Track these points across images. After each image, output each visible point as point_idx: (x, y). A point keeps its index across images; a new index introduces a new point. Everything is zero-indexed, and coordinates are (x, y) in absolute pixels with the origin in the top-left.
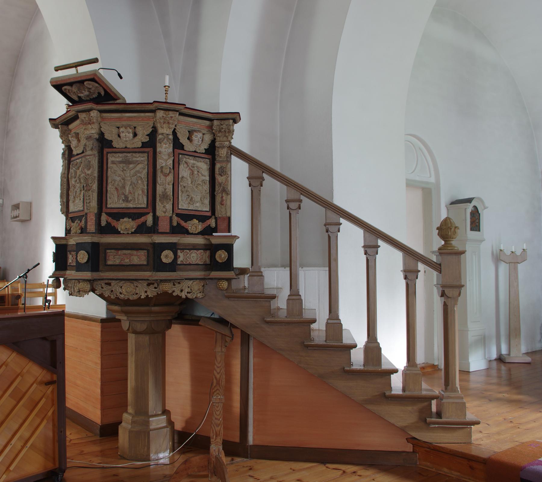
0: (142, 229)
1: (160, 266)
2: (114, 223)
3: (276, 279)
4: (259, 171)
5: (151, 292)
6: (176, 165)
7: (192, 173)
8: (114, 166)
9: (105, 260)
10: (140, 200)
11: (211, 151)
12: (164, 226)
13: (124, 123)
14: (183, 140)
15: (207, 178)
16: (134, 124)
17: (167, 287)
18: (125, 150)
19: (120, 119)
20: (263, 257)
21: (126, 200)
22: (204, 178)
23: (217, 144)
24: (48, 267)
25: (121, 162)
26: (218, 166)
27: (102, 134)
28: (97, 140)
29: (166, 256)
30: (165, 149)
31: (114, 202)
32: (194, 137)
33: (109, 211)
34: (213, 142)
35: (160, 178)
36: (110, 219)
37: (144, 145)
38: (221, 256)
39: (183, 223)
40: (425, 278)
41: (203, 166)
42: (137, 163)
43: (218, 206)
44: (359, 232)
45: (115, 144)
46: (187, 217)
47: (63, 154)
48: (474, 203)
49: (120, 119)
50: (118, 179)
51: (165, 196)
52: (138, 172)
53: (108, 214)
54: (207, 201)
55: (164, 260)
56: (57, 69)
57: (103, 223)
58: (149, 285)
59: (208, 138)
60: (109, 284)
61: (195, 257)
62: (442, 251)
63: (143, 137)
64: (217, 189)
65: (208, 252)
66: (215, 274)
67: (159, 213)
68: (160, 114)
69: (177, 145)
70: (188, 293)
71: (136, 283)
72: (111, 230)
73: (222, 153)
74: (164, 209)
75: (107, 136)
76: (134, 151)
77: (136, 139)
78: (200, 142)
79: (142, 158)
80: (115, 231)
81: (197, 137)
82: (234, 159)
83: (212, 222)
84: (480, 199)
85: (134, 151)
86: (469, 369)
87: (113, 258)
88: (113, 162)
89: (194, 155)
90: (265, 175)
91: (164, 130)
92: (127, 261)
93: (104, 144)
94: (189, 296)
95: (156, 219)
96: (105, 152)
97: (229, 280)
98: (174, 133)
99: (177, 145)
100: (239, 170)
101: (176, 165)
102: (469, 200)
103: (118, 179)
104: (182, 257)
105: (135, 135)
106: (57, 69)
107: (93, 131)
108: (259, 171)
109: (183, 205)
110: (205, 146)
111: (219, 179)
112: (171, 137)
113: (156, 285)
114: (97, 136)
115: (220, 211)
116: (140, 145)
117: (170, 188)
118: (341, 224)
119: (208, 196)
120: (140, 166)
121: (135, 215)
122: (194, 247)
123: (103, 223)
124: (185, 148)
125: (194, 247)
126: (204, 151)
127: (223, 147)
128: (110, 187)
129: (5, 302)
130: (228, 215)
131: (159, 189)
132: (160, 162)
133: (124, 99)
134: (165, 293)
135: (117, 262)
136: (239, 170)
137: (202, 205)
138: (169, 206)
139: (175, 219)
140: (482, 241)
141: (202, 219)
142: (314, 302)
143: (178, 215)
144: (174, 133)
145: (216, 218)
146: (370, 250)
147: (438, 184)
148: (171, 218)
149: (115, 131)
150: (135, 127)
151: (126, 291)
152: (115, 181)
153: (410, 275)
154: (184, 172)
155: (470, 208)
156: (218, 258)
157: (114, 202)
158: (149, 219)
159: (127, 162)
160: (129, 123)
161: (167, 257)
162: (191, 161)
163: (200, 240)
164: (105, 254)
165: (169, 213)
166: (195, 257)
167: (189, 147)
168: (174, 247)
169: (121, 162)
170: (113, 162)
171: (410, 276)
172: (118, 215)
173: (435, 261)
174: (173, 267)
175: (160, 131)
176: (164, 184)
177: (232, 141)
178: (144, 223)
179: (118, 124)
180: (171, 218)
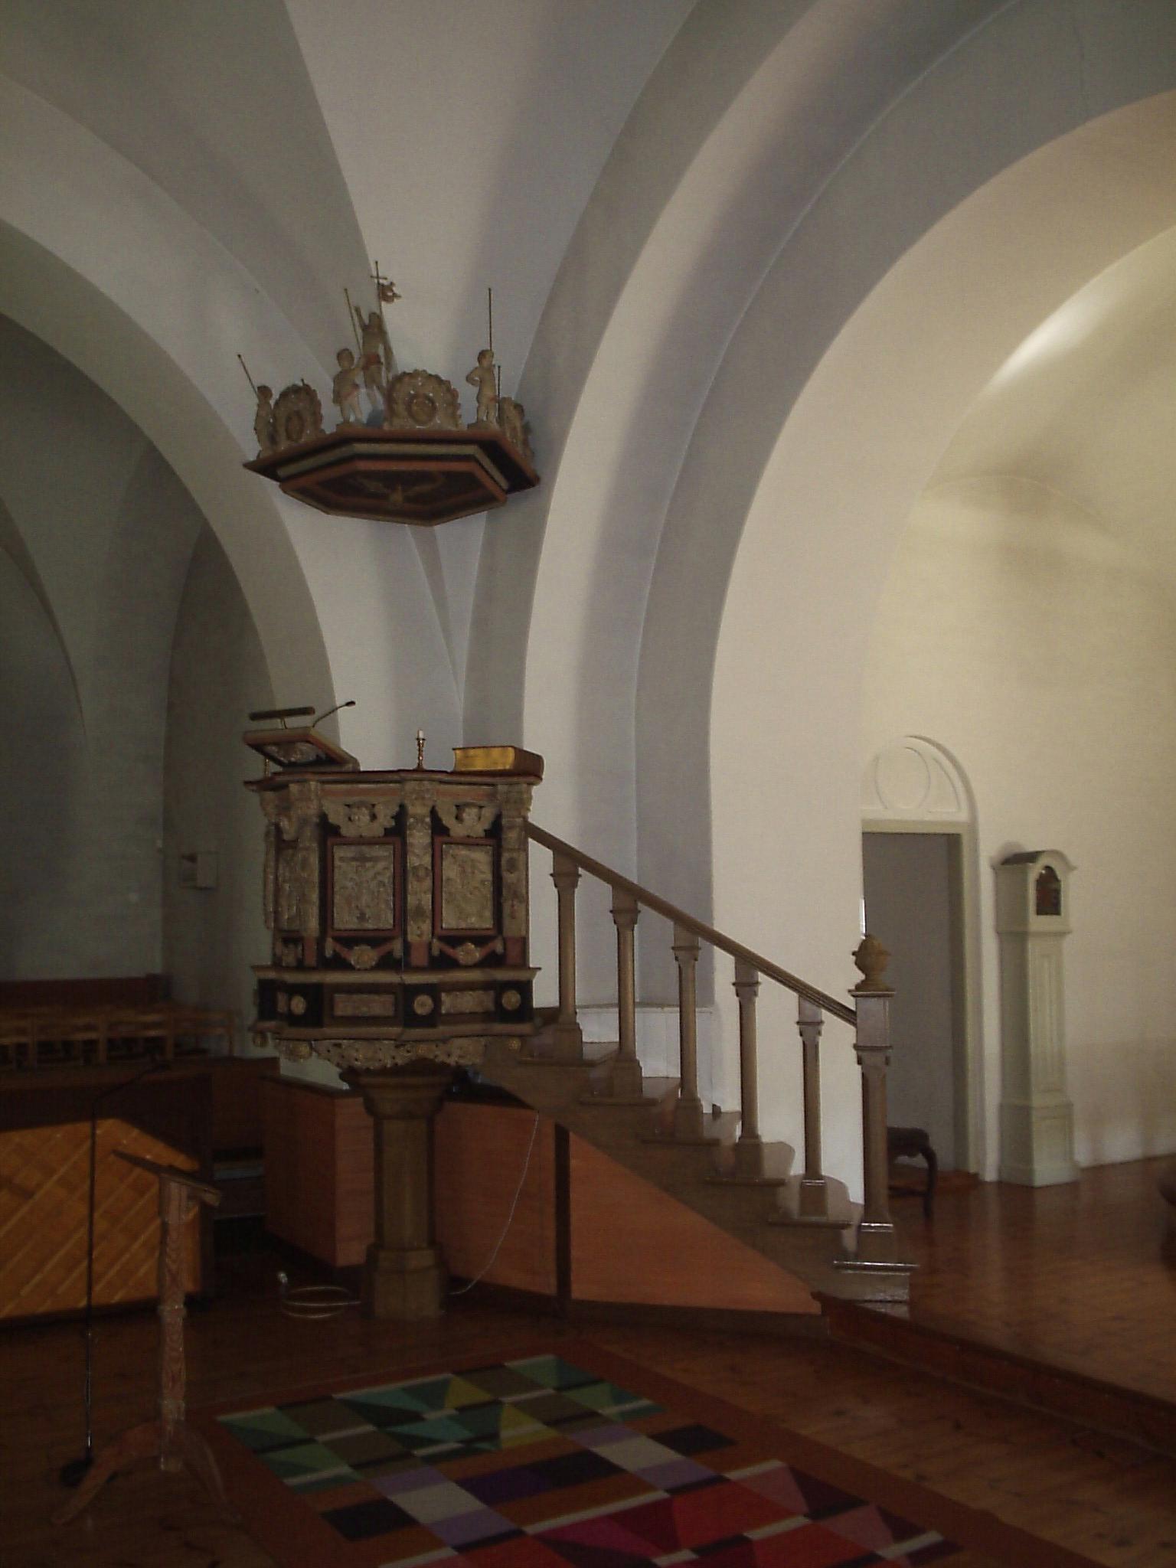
0: (387, 963)
1: (411, 1020)
2: (344, 952)
4: (570, 864)
5: (402, 1057)
6: (436, 858)
7: (464, 871)
8: (344, 865)
9: (332, 1008)
11: (495, 833)
12: (419, 958)
13: (356, 799)
14: (448, 820)
15: (489, 876)
16: (372, 800)
17: (422, 1050)
18: (361, 841)
19: (349, 793)
20: (580, 996)
21: (362, 917)
22: (483, 876)
23: (504, 821)
24: (251, 1013)
25: (354, 859)
26: (506, 856)
27: (323, 817)
28: (318, 825)
29: (423, 1005)
30: (419, 838)
31: (345, 919)
32: (465, 816)
33: (337, 934)
34: (498, 818)
35: (413, 885)
36: (338, 948)
37: (388, 832)
38: (511, 999)
39: (449, 951)
41: (481, 858)
42: (375, 860)
43: (507, 921)
45: (344, 831)
46: (455, 939)
47: (267, 834)
48: (1043, 861)
49: (349, 793)
50: (350, 884)
51: (419, 911)
52: (379, 873)
53: (337, 939)
54: (488, 914)
55: (419, 1011)
56: (255, 717)
57: (329, 953)
58: (397, 1047)
59: (488, 813)
60: (339, 1046)
61: (468, 1002)
62: (859, 991)
63: (385, 820)
64: (505, 892)
65: (492, 993)
66: (498, 1028)
68: (410, 786)
69: (438, 829)
70: (460, 1057)
71: (377, 1044)
73: (511, 836)
74: (419, 931)
75: (333, 819)
76: (371, 842)
77: (376, 824)
78: (474, 823)
79: (384, 852)
80: (454, 964)
81: (470, 814)
82: (532, 842)
83: (498, 947)
84: (1057, 854)
85: (371, 842)
86: (1030, 1173)
87: (344, 1006)
88: (341, 859)
89: (469, 842)
90: (581, 871)
91: (418, 810)
92: (364, 1010)
93: (328, 831)
94: (462, 1062)
95: (407, 947)
96: (329, 843)
97: (521, 1037)
98: (433, 813)
99: (438, 829)
100: (540, 860)
101: (436, 858)
102: (1033, 857)
103: (350, 884)
104: (448, 1002)
105: (374, 817)
106: (255, 717)
107: (312, 810)
108: (570, 864)
109: (450, 921)
111: (509, 877)
112: (428, 820)
113: (408, 1047)
114: (315, 820)
115: (510, 928)
116: (381, 832)
117: (427, 898)
118: (699, 949)
119: (490, 904)
120: (380, 866)
121: (374, 939)
122: (470, 986)
123: (329, 953)
124: (452, 833)
125: (470, 986)
126: (482, 834)
127: (511, 827)
128: (337, 899)
130: (523, 933)
131: (411, 900)
132: (413, 861)
133: (355, 762)
134: (423, 1060)
135: (349, 1012)
136: (540, 860)
137: (480, 919)
138: (426, 926)
139: (437, 945)
140: (1061, 934)
141: (480, 940)
143: (441, 938)
144: (433, 813)
145: (505, 941)
146: (745, 989)
147: (973, 825)
148: (430, 945)
149: (343, 811)
150: (374, 805)
151: (361, 1055)
152: (344, 888)
154: (450, 870)
155: (1035, 871)
156: (509, 1002)
157: (345, 919)
158: (397, 947)
159: (362, 859)
160: (363, 798)
161: (423, 1005)
162: (463, 852)
164: (332, 1000)
165: (427, 936)
166: (468, 1002)
167: (457, 830)
168: (433, 991)
169: (354, 859)
170: (341, 859)
171: (809, 1030)
172: (350, 940)
173: (824, 1011)
174: (431, 1019)
175: (411, 810)
176: (419, 894)
177: (529, 814)
178: (390, 953)
179: (350, 800)
180: (430, 945)
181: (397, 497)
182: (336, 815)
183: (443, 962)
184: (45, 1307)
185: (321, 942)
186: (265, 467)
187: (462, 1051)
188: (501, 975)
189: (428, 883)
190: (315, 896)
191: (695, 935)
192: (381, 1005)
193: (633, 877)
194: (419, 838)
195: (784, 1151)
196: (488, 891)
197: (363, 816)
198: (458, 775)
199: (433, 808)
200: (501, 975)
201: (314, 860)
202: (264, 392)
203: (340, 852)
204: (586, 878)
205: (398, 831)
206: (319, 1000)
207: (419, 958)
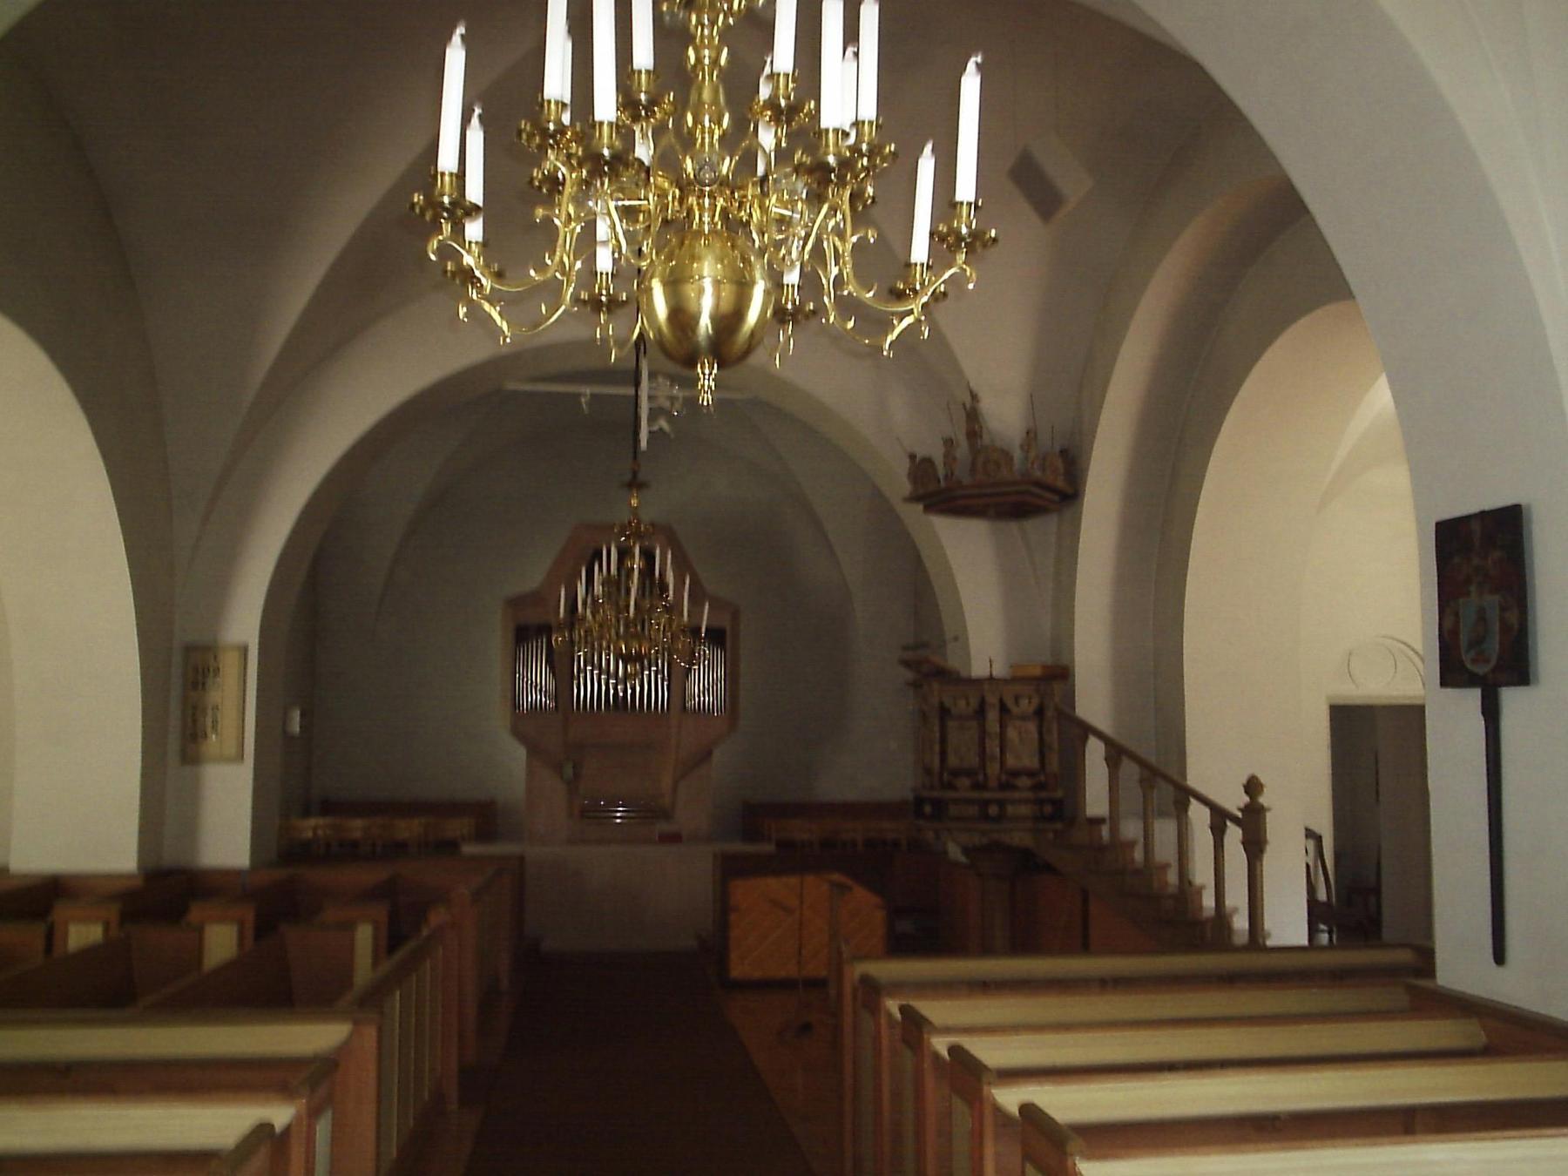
0: (977, 786)
1: (986, 817)
3: (1131, 829)
4: (1116, 754)
5: (985, 841)
6: (1002, 726)
10: (973, 760)
11: (1040, 712)
12: (993, 783)
14: (1010, 703)
30: (992, 716)
31: (953, 761)
40: (1234, 834)
41: (1032, 727)
44: (1171, 788)
46: (1016, 774)
59: (1036, 701)
61: (1024, 810)
63: (974, 703)
67: (989, 771)
69: (1003, 709)
72: (951, 786)
74: (993, 769)
78: (1027, 706)
80: (1014, 788)
81: (1024, 702)
83: (1042, 778)
87: (953, 810)
89: (1024, 718)
91: (992, 699)
93: (944, 712)
99: (1003, 709)
104: (1010, 809)
109: (1011, 761)
110: (1031, 709)
121: (969, 773)
129: (522, 859)
138: (997, 766)
139: (1004, 777)
141: (1030, 774)
142: (1165, 849)
153: (1218, 831)
154: (1012, 733)
158: (981, 777)
161: (993, 810)
162: (1018, 723)
163: (1030, 795)
166: (1024, 810)
167: (1015, 710)
168: (1001, 804)
172: (956, 773)
174: (1001, 817)
176: (993, 747)
181: (82, 934)
182: (948, 702)
183: (1004, 786)
184: (757, 974)
185: (941, 774)
186: (914, 498)
187: (1020, 837)
188: (1043, 795)
189: (997, 742)
190: (937, 748)
191: (1184, 795)
192: (973, 810)
193: (1153, 760)
194: (992, 716)
195: (1131, 845)
196: (1036, 744)
197: (962, 703)
198: (1014, 680)
199: (1307, 829)
200: (1043, 795)
201: (937, 728)
202: (912, 457)
203: (951, 724)
204: (1126, 762)
205: (981, 712)
206: (940, 806)
207: (993, 783)
